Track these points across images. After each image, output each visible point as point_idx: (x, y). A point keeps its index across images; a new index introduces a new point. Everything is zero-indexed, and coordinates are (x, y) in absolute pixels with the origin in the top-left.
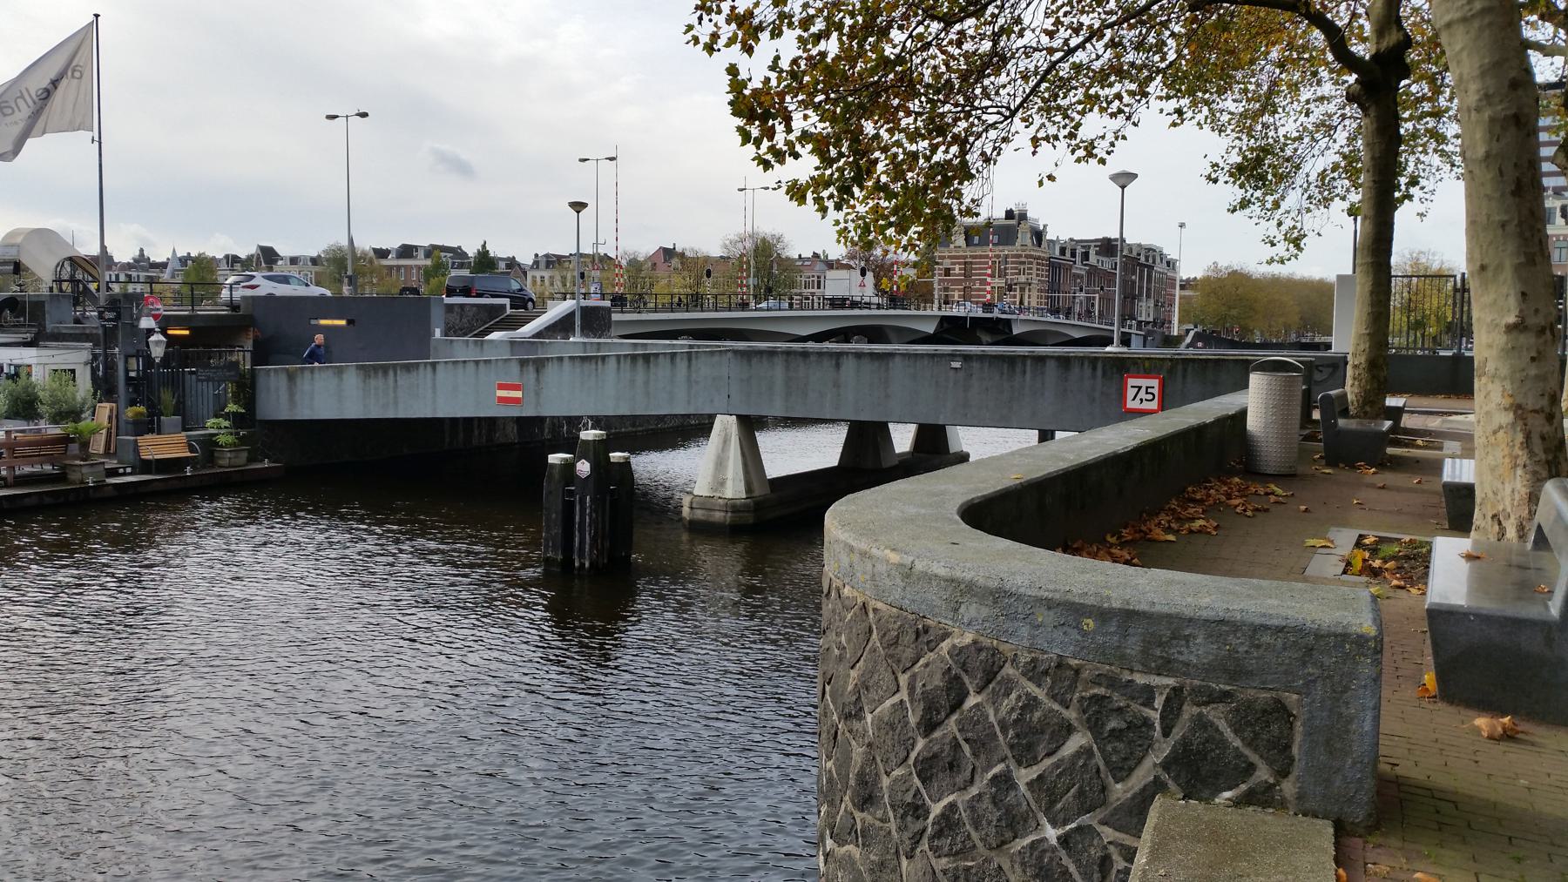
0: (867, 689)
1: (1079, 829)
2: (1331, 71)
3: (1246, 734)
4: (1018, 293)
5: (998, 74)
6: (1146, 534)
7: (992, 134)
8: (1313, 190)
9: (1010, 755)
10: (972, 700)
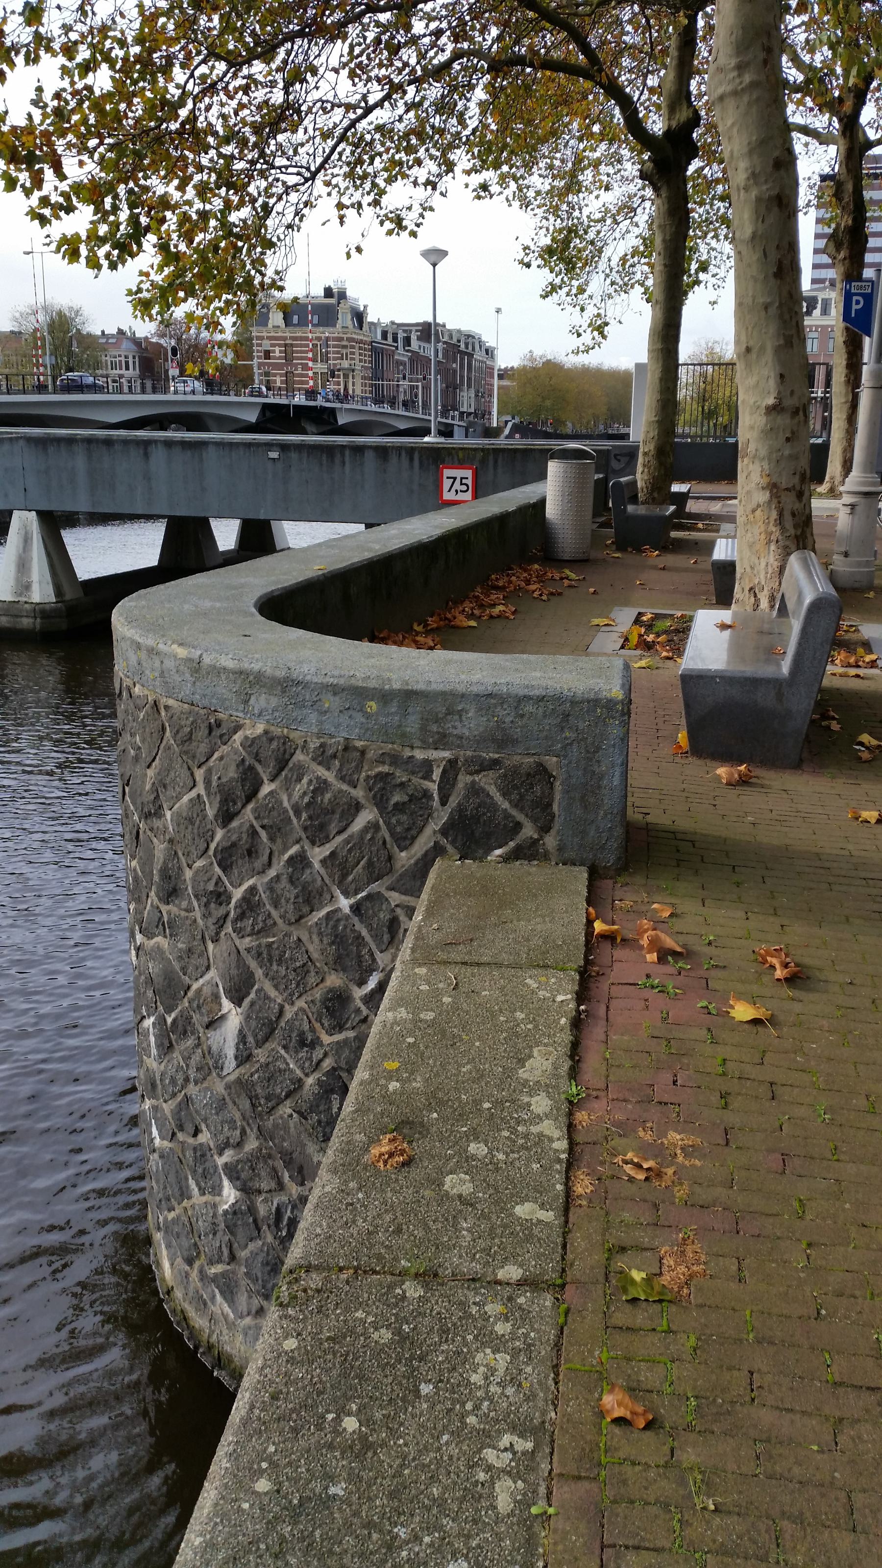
0: (165, 786)
1: (369, 897)
2: (632, 150)
3: (513, 797)
4: (341, 380)
5: (294, 131)
6: (450, 621)
7: (293, 197)
8: (615, 276)
9: (304, 836)
10: (267, 788)
